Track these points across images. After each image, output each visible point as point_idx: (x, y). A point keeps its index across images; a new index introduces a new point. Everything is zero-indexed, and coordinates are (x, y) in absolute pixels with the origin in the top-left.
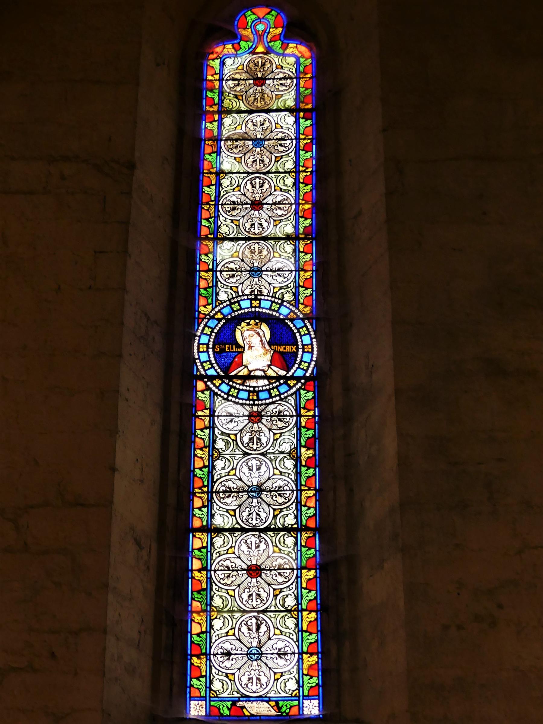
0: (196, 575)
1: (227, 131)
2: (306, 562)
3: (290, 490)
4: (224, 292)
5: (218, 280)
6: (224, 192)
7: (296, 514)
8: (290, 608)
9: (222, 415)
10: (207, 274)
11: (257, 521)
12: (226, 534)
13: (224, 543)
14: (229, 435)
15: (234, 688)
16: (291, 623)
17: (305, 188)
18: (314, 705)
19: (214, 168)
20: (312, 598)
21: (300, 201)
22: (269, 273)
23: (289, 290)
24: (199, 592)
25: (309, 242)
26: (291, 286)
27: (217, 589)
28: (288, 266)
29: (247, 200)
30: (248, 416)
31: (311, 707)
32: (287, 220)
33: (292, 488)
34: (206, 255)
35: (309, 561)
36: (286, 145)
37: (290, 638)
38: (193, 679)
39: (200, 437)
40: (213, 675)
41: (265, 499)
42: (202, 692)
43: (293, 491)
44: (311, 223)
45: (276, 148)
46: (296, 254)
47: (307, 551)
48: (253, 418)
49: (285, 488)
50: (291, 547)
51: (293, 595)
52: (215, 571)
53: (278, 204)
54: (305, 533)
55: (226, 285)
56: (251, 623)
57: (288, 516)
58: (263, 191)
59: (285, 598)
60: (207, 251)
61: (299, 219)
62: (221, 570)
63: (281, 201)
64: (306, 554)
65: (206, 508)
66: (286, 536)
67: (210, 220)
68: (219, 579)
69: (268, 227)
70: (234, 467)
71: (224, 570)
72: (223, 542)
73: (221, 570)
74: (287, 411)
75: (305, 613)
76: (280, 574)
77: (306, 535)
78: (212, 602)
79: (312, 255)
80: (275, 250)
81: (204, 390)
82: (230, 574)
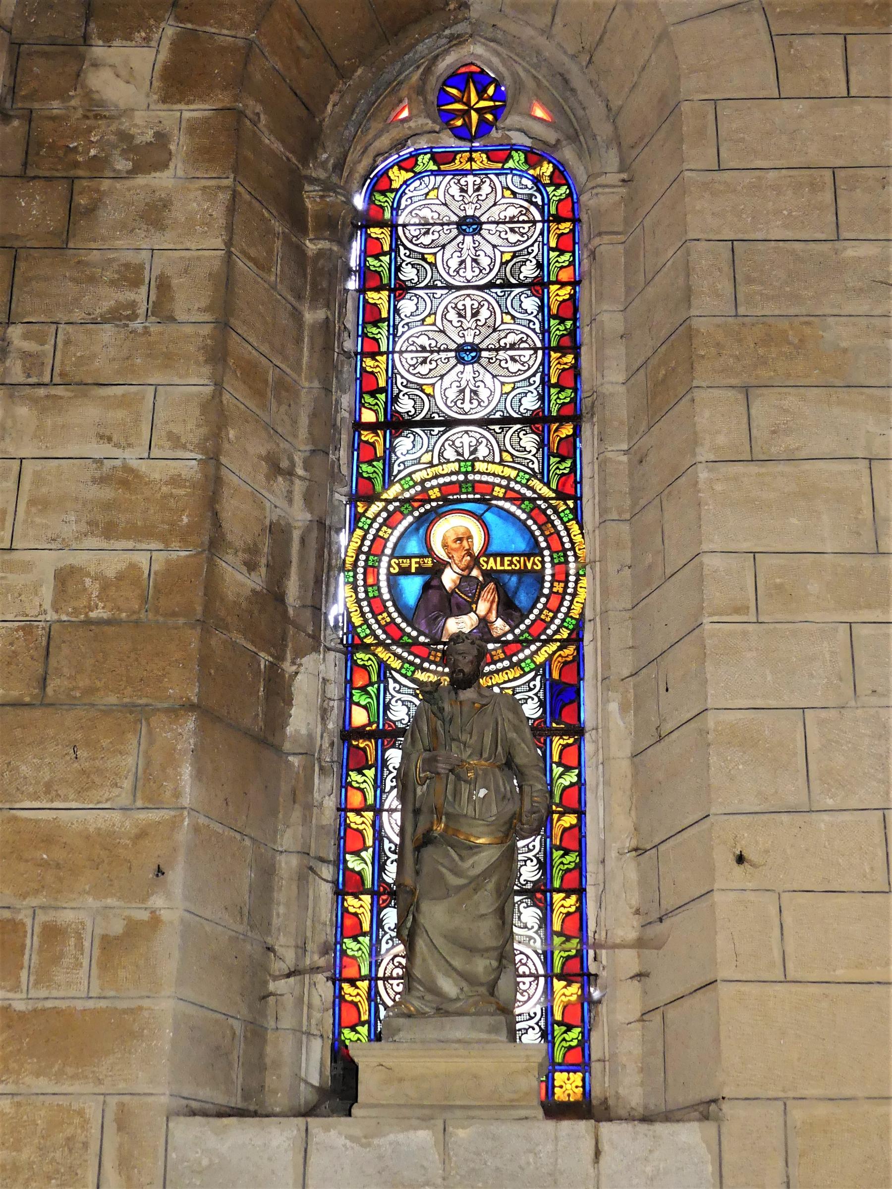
0: (349, 946)
1: (409, 201)
2: (563, 922)
3: (531, 975)
5: (396, 371)
6: (403, 327)
7: (543, 1027)
9: (412, 222)
10: (380, 295)
11: (471, 403)
12: (418, 430)
13: (417, 309)
14: (420, 387)
15: (436, 302)
16: (531, 304)
17: (560, 260)
19: (369, 847)
21: (554, 807)
22: (492, 227)
24: (373, 394)
25: (571, 741)
28: (529, 341)
29: (449, 342)
30: (455, 350)
32: (526, 383)
33: (536, 969)
34: (353, 1029)
35: (560, 205)
36: (523, 359)
37: (529, 328)
39: (357, 785)
41: (488, 237)
42: (380, 381)
43: (536, 349)
44: (568, 191)
45: (503, 235)
46: (544, 368)
47: (558, 256)
48: (464, 227)
49: (523, 345)
50: (533, 927)
52: (401, 352)
53: (509, 349)
54: (558, 738)
55: (415, 252)
56: (464, 305)
57: (526, 1033)
58: (479, 323)
61: (551, 853)
62: (411, 351)
63: (514, 217)
64: (557, 261)
65: (384, 395)
67: (369, 689)
68: (407, 366)
69: (490, 399)
70: (430, 448)
71: (417, 351)
72: (415, 308)
73: (411, 351)
74: (525, 964)
76: (512, 230)
79: (574, 255)
80: (503, 308)
82: (426, 358)
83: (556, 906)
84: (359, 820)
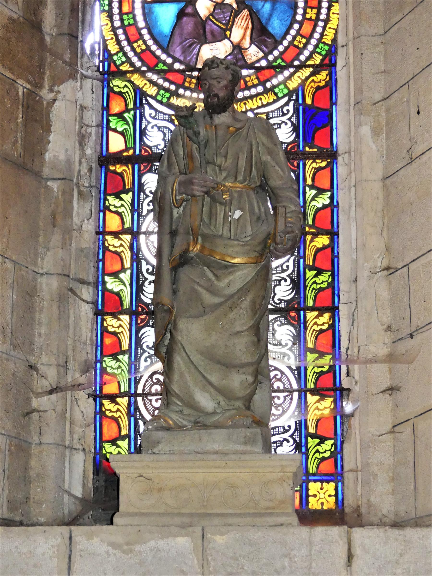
0: (109, 364)
4: (155, 128)
8: (283, 305)
18: (327, 494)
19: (130, 148)
20: (326, 327)
23: (284, 275)
25: (324, 164)
26: (288, 111)
27: (153, 115)
31: (322, 496)
34: (113, 442)
38: (108, 197)
40: (146, 120)
47: (319, 444)
51: (289, 124)
54: (311, 161)
59: (277, 447)
60: (117, 267)
66: (279, 323)
75: (311, 315)
77: (314, 165)
78: (144, 138)
81: (123, 112)
83: (310, 324)
84: (117, 243)
